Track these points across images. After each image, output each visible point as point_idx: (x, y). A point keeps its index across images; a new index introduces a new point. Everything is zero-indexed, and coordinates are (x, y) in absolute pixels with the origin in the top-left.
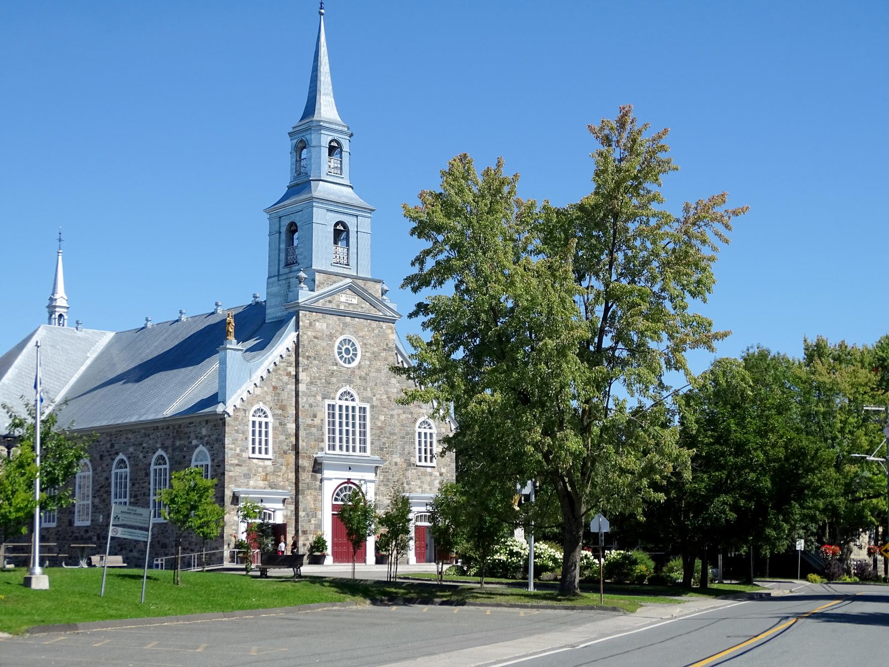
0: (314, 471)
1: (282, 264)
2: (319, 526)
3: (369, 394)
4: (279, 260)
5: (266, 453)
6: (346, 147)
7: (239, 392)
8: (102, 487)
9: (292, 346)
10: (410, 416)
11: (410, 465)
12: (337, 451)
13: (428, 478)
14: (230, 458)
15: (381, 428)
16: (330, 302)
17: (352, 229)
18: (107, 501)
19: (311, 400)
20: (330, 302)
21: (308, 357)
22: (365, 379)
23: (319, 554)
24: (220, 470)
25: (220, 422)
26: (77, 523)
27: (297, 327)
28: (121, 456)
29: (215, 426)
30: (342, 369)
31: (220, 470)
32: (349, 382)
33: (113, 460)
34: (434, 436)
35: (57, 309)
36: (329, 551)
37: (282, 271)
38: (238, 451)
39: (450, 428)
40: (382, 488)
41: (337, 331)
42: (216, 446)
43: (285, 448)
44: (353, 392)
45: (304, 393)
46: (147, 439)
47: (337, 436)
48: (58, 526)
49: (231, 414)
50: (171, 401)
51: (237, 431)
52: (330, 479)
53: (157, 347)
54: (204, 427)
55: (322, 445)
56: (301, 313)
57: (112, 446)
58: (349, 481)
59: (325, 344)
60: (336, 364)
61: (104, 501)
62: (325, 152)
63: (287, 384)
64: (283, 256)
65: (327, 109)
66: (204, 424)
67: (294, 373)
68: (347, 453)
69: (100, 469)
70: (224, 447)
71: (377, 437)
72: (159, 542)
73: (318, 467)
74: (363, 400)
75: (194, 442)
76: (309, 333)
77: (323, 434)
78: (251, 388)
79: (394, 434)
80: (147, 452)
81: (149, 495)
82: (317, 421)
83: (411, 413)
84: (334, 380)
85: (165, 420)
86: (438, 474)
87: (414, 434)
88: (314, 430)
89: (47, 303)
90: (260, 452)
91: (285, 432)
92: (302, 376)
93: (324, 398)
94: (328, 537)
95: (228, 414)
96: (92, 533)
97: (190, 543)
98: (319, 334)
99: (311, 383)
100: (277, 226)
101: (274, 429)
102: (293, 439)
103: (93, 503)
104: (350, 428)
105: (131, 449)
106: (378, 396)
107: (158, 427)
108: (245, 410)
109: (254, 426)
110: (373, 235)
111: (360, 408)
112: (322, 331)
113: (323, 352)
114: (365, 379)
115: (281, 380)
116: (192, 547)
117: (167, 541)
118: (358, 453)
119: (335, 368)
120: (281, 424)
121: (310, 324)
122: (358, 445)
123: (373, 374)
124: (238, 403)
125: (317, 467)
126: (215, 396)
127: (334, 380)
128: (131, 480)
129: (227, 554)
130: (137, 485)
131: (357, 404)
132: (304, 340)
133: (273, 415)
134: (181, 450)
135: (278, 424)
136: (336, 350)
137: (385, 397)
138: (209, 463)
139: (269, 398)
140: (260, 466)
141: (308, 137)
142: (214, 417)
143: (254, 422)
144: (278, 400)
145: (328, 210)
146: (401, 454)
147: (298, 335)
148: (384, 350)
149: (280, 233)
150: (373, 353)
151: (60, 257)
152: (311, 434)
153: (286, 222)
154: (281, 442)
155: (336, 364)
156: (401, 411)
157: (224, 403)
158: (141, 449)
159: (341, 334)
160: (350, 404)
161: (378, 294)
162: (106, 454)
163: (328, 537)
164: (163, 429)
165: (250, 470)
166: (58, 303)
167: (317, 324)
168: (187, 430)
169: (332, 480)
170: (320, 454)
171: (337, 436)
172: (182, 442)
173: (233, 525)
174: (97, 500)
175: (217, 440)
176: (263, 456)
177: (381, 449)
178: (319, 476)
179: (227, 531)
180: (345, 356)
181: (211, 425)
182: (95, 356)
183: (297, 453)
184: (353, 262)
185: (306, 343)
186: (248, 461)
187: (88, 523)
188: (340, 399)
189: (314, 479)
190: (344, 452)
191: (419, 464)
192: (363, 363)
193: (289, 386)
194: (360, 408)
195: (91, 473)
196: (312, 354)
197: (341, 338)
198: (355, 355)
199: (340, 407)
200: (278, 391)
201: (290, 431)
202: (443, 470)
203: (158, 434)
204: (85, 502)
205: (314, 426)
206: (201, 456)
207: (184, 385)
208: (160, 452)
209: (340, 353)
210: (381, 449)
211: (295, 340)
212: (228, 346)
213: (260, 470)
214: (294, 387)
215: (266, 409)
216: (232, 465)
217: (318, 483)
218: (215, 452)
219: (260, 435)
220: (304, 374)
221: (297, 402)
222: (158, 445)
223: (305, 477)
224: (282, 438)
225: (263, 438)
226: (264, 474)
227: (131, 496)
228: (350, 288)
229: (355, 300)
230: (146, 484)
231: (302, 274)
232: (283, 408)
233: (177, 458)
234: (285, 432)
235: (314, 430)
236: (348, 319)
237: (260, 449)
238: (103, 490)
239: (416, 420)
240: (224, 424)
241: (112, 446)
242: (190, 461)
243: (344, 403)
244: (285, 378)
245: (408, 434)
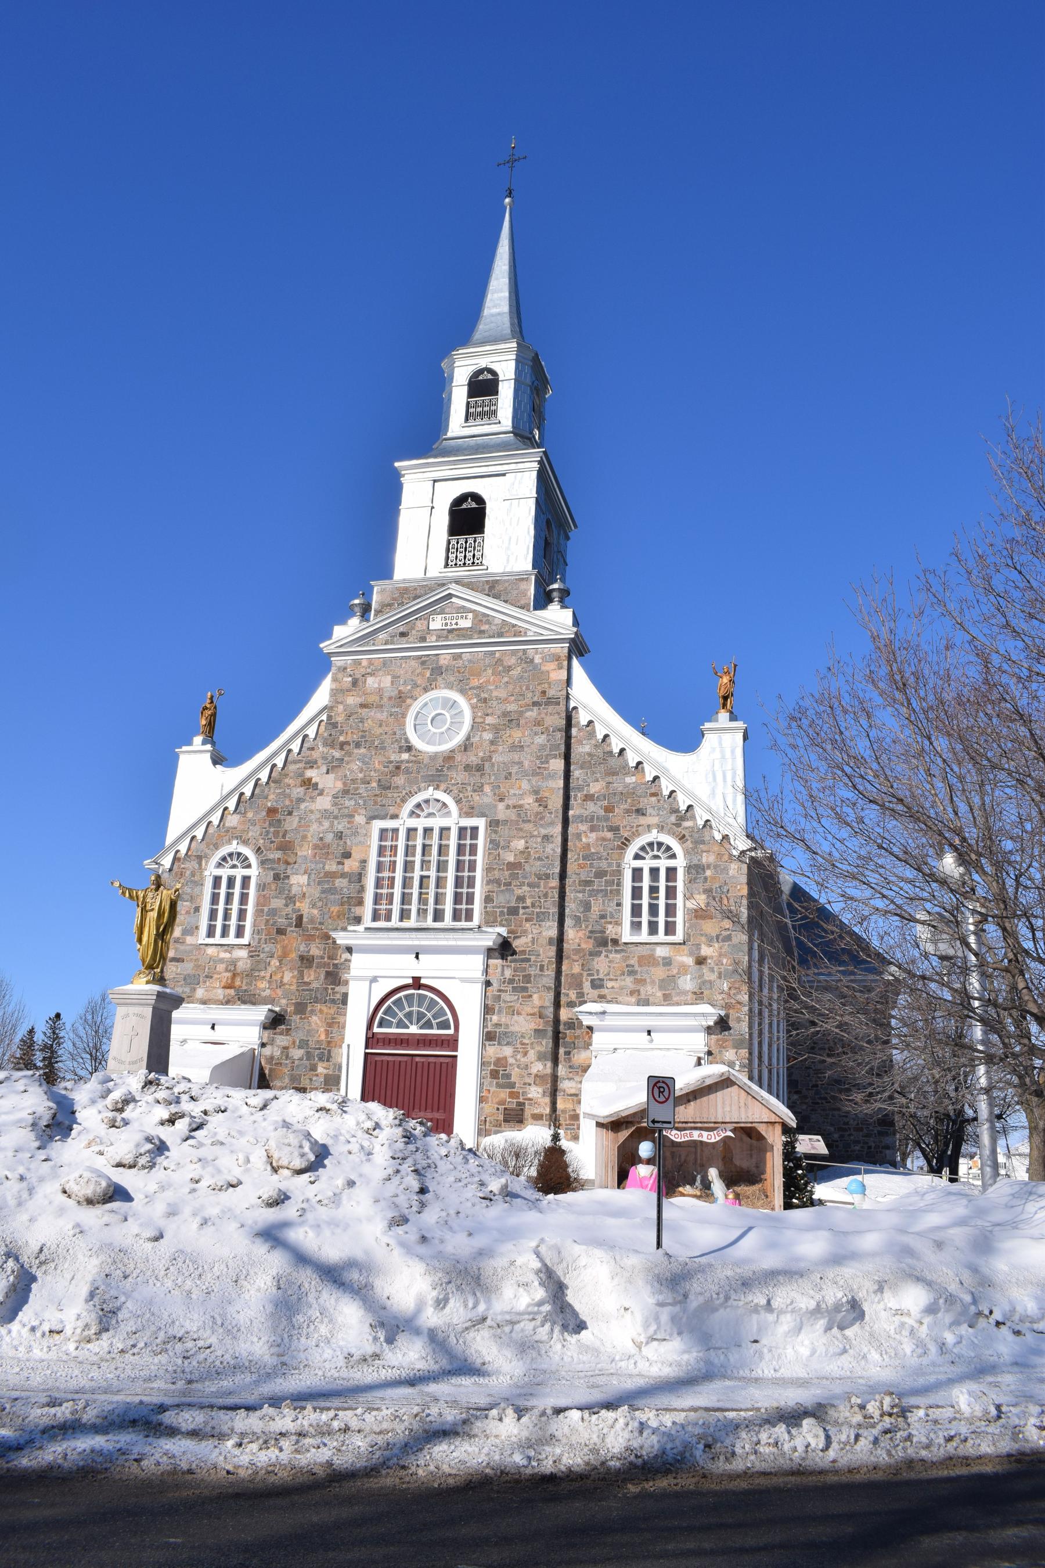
5: (240, 933)
10: (609, 835)
13: (659, 973)
34: (680, 874)
39: (84, 1421)
43: (281, 921)
58: (417, 983)
77: (362, 889)
82: (351, 865)
86: (690, 961)
87: (619, 873)
88: (340, 883)
99: (346, 792)
101: (262, 887)
119: (405, 756)
120: (277, 877)
121: (355, 683)
127: (400, 780)
133: (262, 863)
135: (270, 878)
139: (254, 832)
140: (222, 961)
150: (505, 714)
152: (332, 891)
160: (437, 823)
176: (231, 939)
192: (475, 740)
202: (705, 951)
205: (343, 875)
210: (513, 911)
215: (247, 852)
225: (235, 906)
235: (340, 883)
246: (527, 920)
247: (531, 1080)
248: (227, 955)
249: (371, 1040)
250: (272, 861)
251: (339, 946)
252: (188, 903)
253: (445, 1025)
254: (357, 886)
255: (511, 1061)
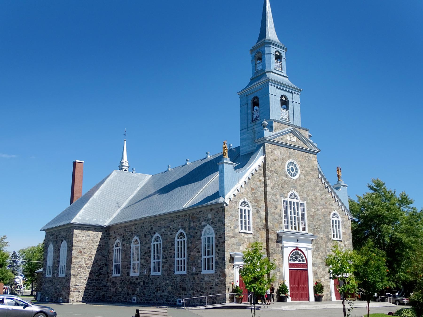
0: (277, 242)
1: (250, 121)
2: (282, 277)
3: (306, 196)
4: (247, 120)
6: (284, 56)
7: (232, 190)
8: (146, 253)
9: (261, 164)
10: (327, 210)
11: (329, 239)
12: (290, 230)
14: (228, 233)
15: (313, 216)
16: (282, 139)
17: (290, 100)
18: (149, 261)
19: (274, 198)
20: (282, 139)
21: (271, 171)
22: (303, 187)
23: (284, 295)
24: (221, 240)
25: (220, 209)
26: (132, 275)
27: (264, 153)
28: (157, 234)
29: (217, 212)
30: (290, 179)
31: (221, 240)
32: (295, 188)
33: (152, 237)
35: (124, 167)
36: (289, 293)
37: (249, 125)
38: (232, 228)
40: (315, 253)
41: (286, 157)
42: (218, 225)
43: (260, 227)
44: (297, 194)
45: (270, 193)
46: (173, 223)
47: (290, 220)
48: (121, 276)
49: (228, 204)
50: (186, 202)
51: (232, 215)
52: (287, 247)
53: (174, 177)
54: (213, 211)
55: (281, 225)
56: (266, 144)
57: (152, 229)
59: (280, 164)
60: (287, 177)
61: (147, 261)
62: (273, 57)
63: (259, 187)
64: (250, 117)
65: (271, 33)
66: (209, 211)
67: (263, 181)
68: (295, 231)
69: (145, 242)
70: (224, 225)
71: (311, 221)
72: (180, 286)
73: (280, 239)
74: (302, 199)
75: (203, 223)
76: (271, 157)
77: (281, 219)
78: (239, 188)
79: (320, 220)
80: (173, 231)
81: (174, 257)
82: (278, 211)
83: (328, 208)
84: (286, 186)
85: (184, 210)
86: (343, 245)
88: (276, 216)
89: (119, 165)
90: (245, 229)
91: (259, 217)
92: (268, 182)
93: (281, 197)
94: (287, 284)
95: (226, 204)
96: (140, 280)
97: (201, 288)
98: (277, 158)
99: (274, 187)
100: (245, 101)
101: (253, 214)
102: (264, 221)
103: (141, 262)
104: (296, 216)
105: (163, 230)
106: (310, 197)
107: (179, 216)
108: (236, 202)
109: (241, 212)
110: (302, 105)
111: (301, 204)
112: (278, 156)
113: (279, 169)
114: (303, 187)
115: (256, 184)
116: (203, 291)
117: (186, 286)
118: (301, 231)
119: (286, 179)
120: (257, 212)
121: (272, 151)
122: (301, 227)
123: (307, 184)
124: (232, 197)
125: (279, 239)
126: (218, 193)
127: (286, 186)
128: (163, 248)
129: (228, 296)
130: (166, 252)
131: (299, 201)
132: (268, 161)
133: (252, 206)
134: (195, 229)
135: (255, 212)
136: (286, 168)
137: (314, 198)
138: (214, 236)
139: (249, 195)
141: (262, 50)
142: (216, 206)
143: (241, 210)
144: (255, 196)
145: (277, 88)
146: (324, 233)
147: (265, 158)
148: (312, 170)
149: (247, 104)
150: (306, 171)
151: (125, 143)
153: (251, 98)
154: (257, 223)
155: (287, 177)
156: (322, 207)
157: (223, 197)
158: (169, 229)
159: (289, 159)
161: (307, 137)
162: (148, 233)
163: (287, 284)
164: (182, 216)
165: (240, 240)
166: (124, 164)
167: (275, 151)
168: (198, 216)
169: (288, 247)
170: (280, 231)
171: (290, 220)
172: (195, 224)
173: (231, 276)
174: (143, 261)
175: (219, 221)
176: (247, 231)
177: (314, 229)
178: (280, 245)
179: (228, 280)
180: (292, 172)
181: (214, 211)
182: (141, 186)
183: (267, 230)
184: (291, 119)
185: (270, 162)
186: (239, 234)
187: (138, 274)
188: (290, 198)
189: (278, 246)
190: (294, 230)
191: (333, 239)
192: (301, 177)
193: (260, 189)
194: (301, 204)
195: (139, 245)
196: (273, 169)
197: (288, 161)
198: (297, 172)
199: (290, 202)
200: (255, 191)
201: (262, 216)
202: (346, 243)
203: (180, 220)
204: (136, 262)
205: (276, 214)
206: (208, 232)
207: (194, 191)
208: (181, 231)
209: (288, 170)
210: (314, 229)
211: (263, 160)
212: (225, 161)
213: (246, 240)
214: (263, 189)
215: (248, 202)
216: (229, 237)
217: (280, 249)
218: (218, 228)
219: (245, 218)
220: (269, 181)
221: (266, 199)
222: (180, 227)
223: (273, 245)
224: (258, 220)
226: (248, 243)
227: (163, 258)
228: (292, 132)
229: (295, 140)
230: (172, 251)
231: (265, 122)
232: (258, 202)
233: (192, 234)
234: (259, 217)
235: (276, 216)
236: (292, 150)
237: (245, 227)
238: (146, 255)
239: (330, 213)
240: (224, 210)
241: (152, 229)
242: (201, 235)
243: (292, 200)
244: (258, 184)
245: (326, 221)
246: (317, 232)
247: (321, 276)
248: (247, 236)
249: (290, 265)
250: (254, 205)
251: (386, 251)
252: (234, 217)
253: (303, 261)
254: (280, 218)
255: (317, 271)
